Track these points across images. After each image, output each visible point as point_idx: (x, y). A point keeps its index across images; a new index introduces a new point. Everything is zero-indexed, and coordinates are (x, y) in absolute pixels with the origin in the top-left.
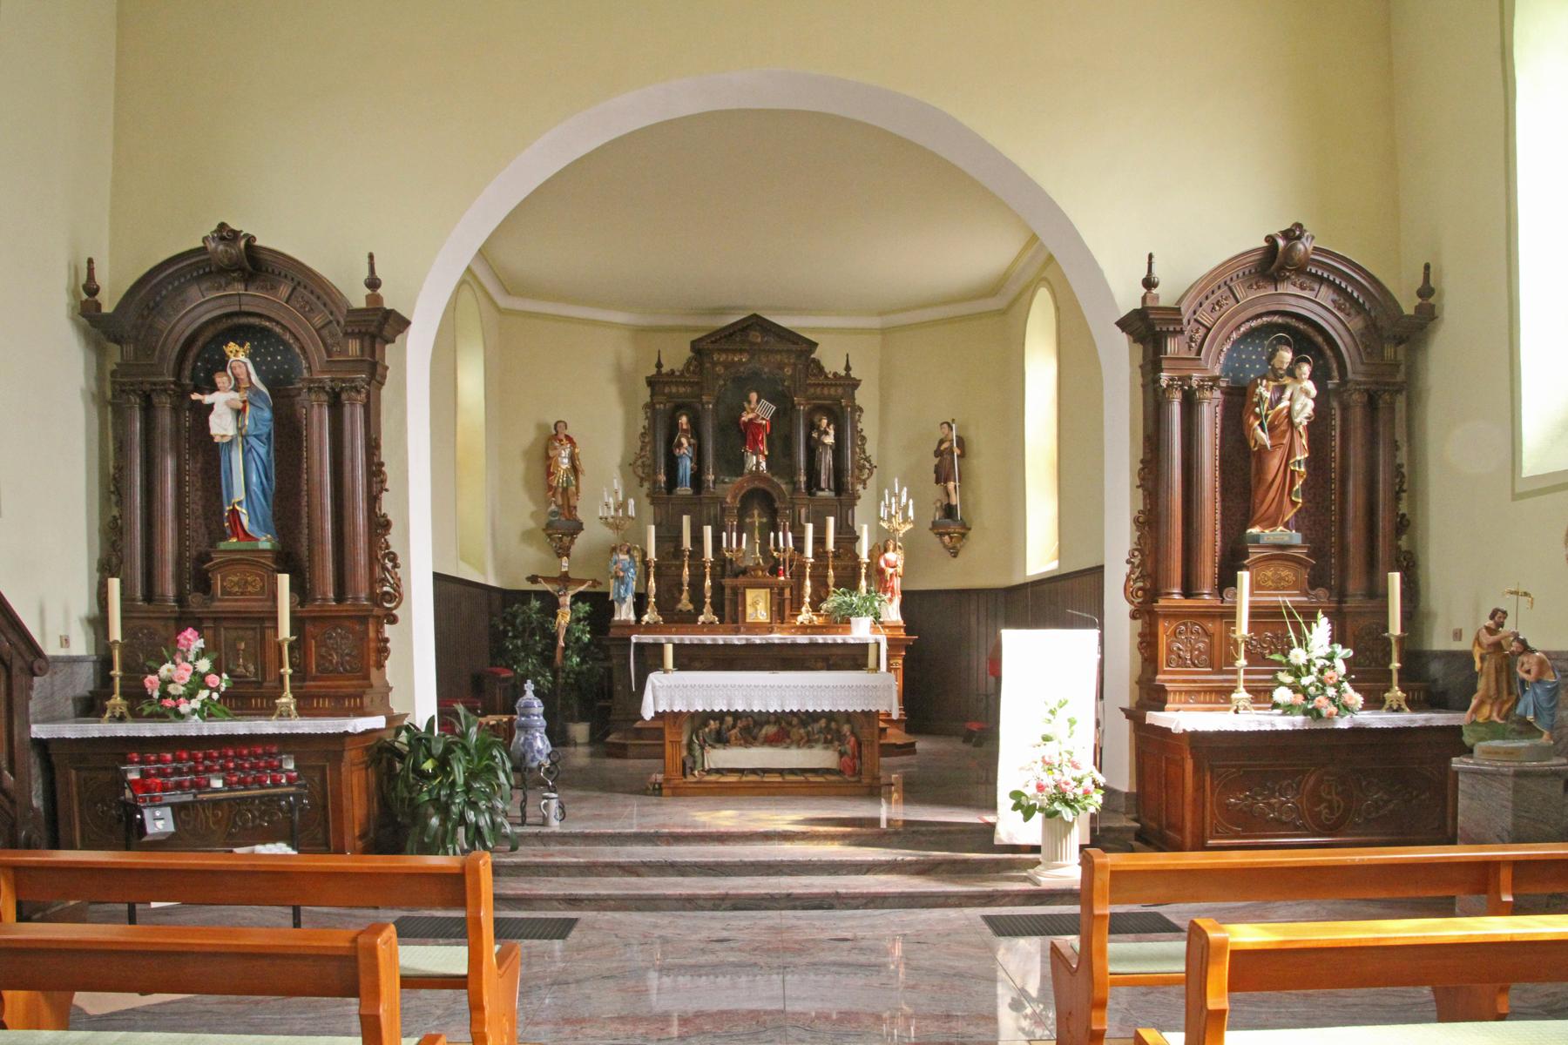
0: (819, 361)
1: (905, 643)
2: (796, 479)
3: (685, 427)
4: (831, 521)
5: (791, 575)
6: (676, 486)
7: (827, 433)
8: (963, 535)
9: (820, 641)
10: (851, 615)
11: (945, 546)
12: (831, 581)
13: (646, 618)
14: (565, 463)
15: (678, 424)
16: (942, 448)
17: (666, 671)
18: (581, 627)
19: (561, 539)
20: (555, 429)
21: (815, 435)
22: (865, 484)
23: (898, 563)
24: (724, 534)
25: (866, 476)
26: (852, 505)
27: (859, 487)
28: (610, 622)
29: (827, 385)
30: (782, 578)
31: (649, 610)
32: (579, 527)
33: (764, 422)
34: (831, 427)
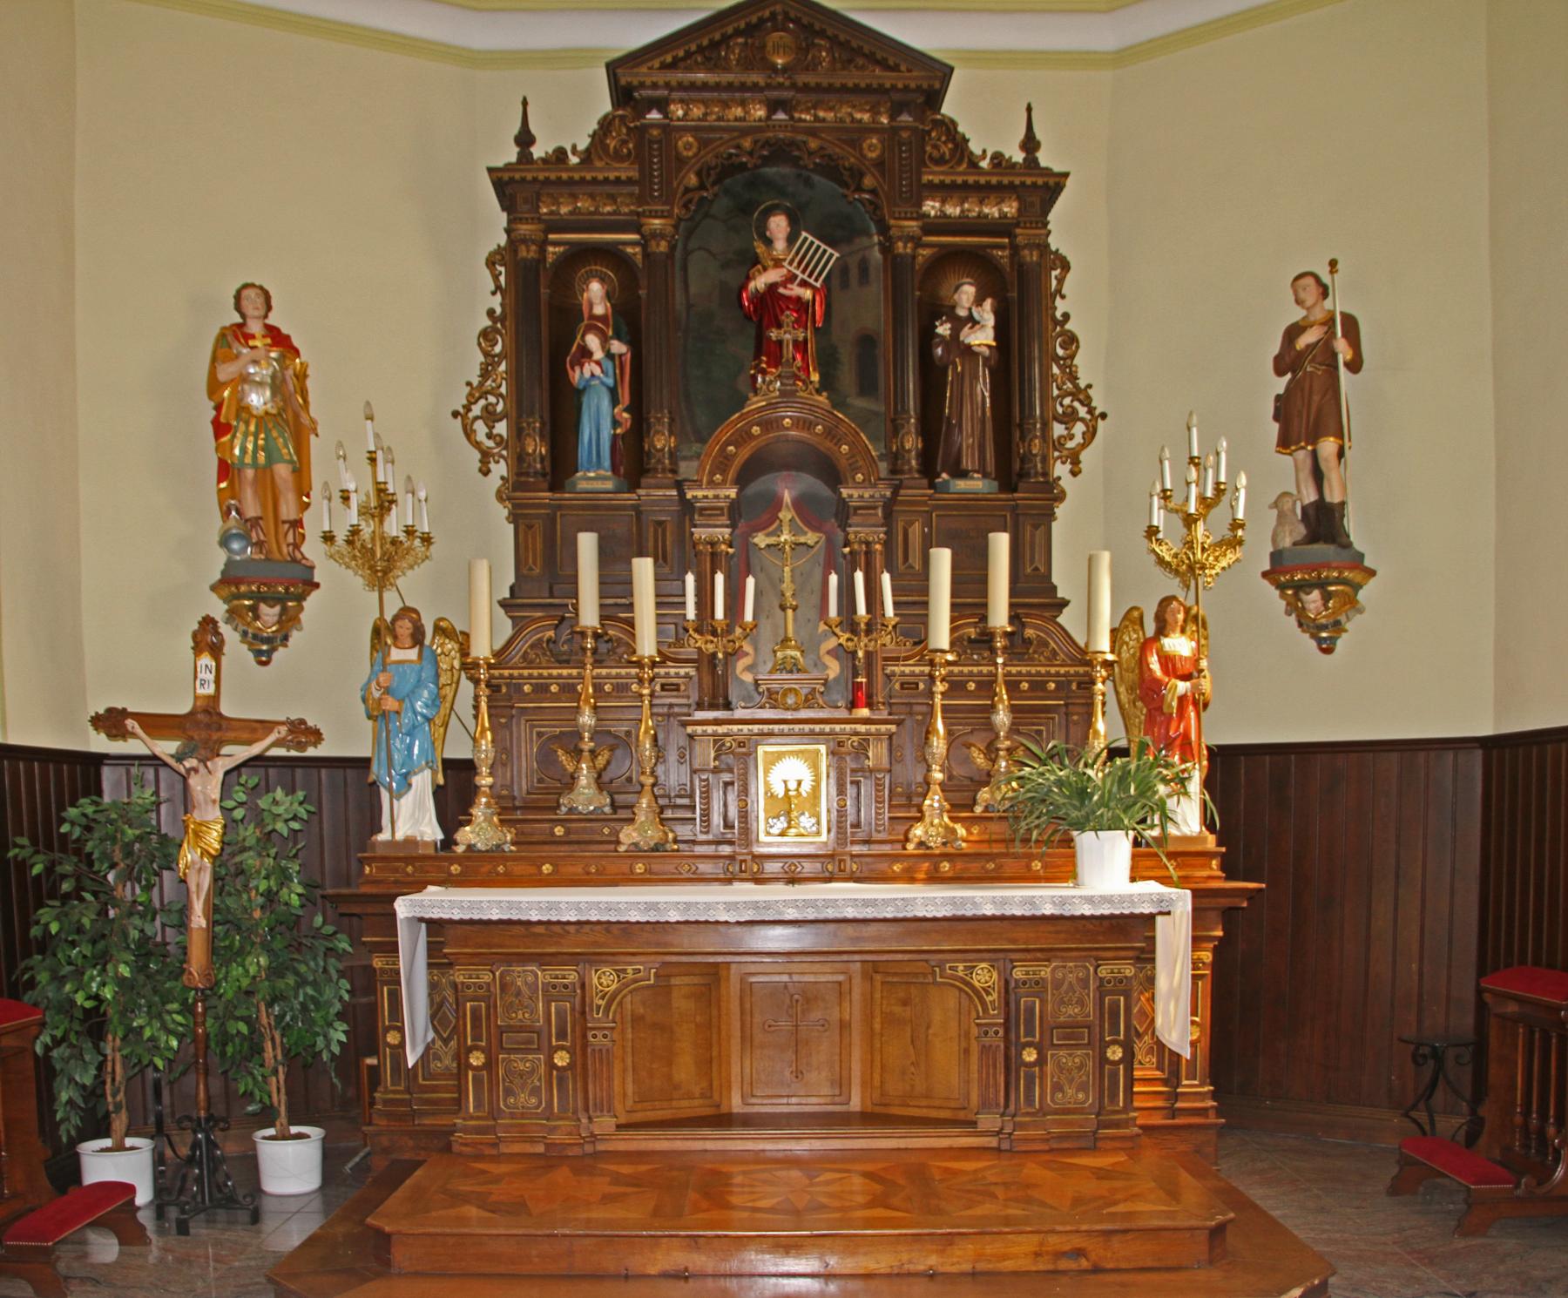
3: (599, 310)
4: (1001, 543)
7: (972, 321)
8: (1357, 587)
12: (1002, 718)
21: (943, 329)
22: (1076, 462)
24: (690, 579)
25: (1078, 439)
27: (1061, 470)
29: (977, 187)
34: (988, 304)
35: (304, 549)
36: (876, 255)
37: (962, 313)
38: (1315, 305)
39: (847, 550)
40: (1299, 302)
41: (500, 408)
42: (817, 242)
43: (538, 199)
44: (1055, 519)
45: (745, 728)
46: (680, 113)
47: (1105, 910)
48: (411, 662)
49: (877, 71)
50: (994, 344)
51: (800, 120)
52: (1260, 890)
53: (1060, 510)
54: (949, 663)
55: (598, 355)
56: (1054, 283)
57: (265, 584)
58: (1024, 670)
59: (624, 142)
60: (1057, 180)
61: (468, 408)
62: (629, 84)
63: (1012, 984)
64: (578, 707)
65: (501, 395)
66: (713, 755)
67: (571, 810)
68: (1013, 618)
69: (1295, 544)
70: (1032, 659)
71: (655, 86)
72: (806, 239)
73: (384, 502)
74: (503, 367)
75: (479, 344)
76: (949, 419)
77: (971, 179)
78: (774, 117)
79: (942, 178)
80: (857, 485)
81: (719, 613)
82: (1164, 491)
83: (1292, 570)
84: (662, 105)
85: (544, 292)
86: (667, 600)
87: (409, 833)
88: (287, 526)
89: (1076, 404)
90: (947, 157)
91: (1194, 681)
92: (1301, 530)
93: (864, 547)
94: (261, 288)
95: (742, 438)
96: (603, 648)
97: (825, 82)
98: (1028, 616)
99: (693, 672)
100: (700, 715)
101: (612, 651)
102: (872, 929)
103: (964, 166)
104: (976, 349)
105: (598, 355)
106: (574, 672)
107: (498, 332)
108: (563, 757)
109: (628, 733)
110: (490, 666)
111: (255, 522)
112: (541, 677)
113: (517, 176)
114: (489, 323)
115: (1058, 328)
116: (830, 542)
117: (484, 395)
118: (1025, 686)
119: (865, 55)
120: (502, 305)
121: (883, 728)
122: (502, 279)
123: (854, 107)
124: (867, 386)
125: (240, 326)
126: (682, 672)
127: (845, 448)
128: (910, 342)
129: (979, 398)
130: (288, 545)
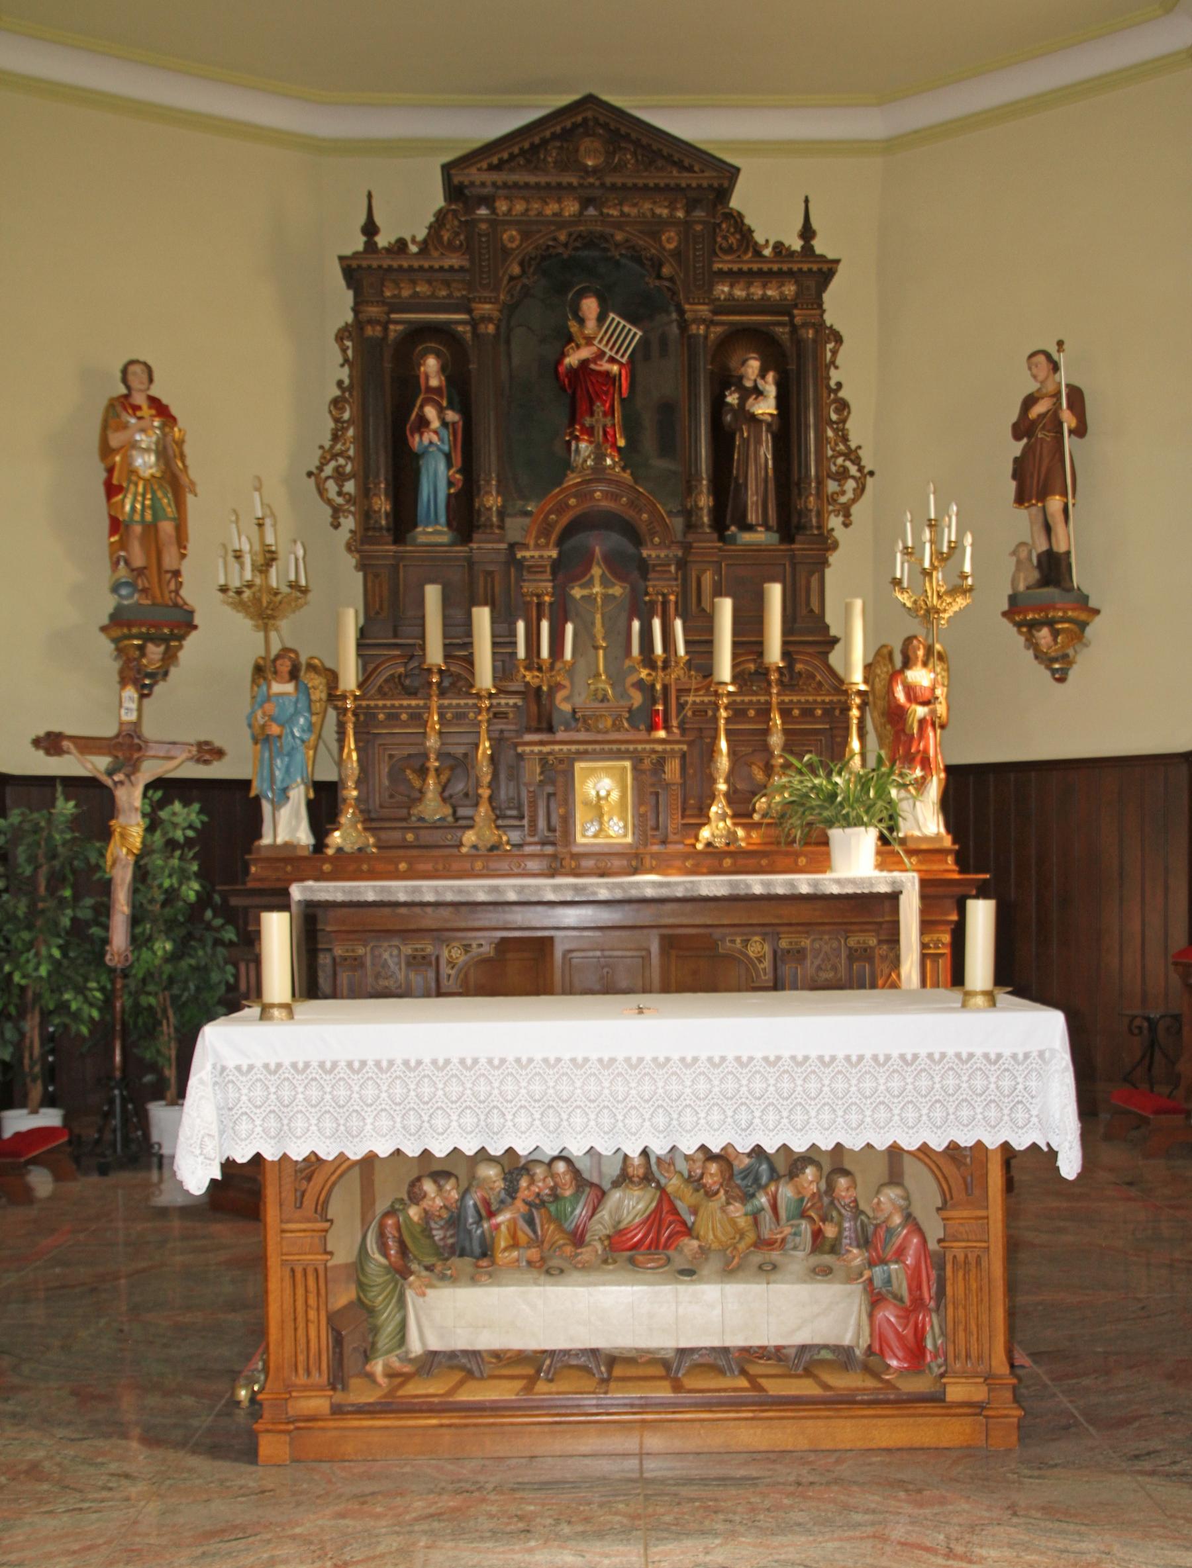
0: (740, 215)
3: (434, 382)
4: (775, 593)
5: (681, 727)
6: (415, 526)
7: (758, 392)
8: (1083, 625)
9: (758, 890)
10: (831, 823)
11: (1039, 656)
12: (776, 740)
14: (146, 463)
15: (417, 377)
17: (265, 1014)
18: (175, 862)
19: (141, 648)
20: (125, 380)
21: (732, 399)
22: (847, 515)
23: (939, 692)
24: (521, 626)
25: (850, 495)
26: (822, 564)
27: (835, 522)
29: (760, 273)
30: (662, 734)
32: (185, 623)
33: (615, 368)
34: (770, 376)
35: (183, 592)
36: (675, 329)
37: (749, 384)
38: (1047, 378)
39: (647, 598)
40: (1035, 377)
41: (348, 469)
42: (623, 323)
43: (383, 285)
44: (829, 565)
45: (565, 748)
46: (504, 208)
47: (850, 890)
48: (287, 694)
49: (675, 173)
50: (775, 412)
51: (608, 215)
52: (985, 881)
53: (833, 558)
54: (730, 694)
55: (435, 424)
56: (829, 355)
57: (154, 626)
58: (795, 699)
59: (457, 234)
60: (830, 266)
61: (321, 469)
62: (461, 183)
63: (779, 953)
64: (425, 733)
65: (349, 458)
66: (538, 770)
67: (421, 819)
68: (786, 655)
69: (1028, 588)
70: (802, 690)
71: (483, 184)
72: (613, 319)
73: (269, 558)
74: (351, 432)
75: (330, 412)
76: (737, 478)
77: (755, 267)
78: (586, 213)
79: (730, 266)
80: (656, 547)
81: (545, 653)
82: (906, 548)
83: (1025, 611)
84: (488, 201)
85: (388, 365)
86: (502, 642)
87: (287, 839)
88: (169, 576)
89: (848, 464)
90: (735, 246)
91: (931, 707)
92: (1035, 575)
93: (660, 598)
94: (145, 364)
95: (562, 508)
96: (446, 684)
97: (630, 182)
98: (798, 653)
99: (520, 703)
100: (528, 737)
101: (453, 684)
102: (669, 907)
103: (750, 254)
104: (762, 417)
105: (435, 424)
106: (421, 703)
107: (346, 401)
108: (410, 775)
109: (466, 755)
110: (356, 698)
111: (140, 572)
112: (393, 706)
113: (364, 264)
114: (338, 393)
115: (832, 396)
116: (634, 590)
117: (334, 457)
118: (796, 712)
119: (663, 157)
120: (351, 377)
121: (676, 747)
122: (350, 353)
123: (654, 203)
124: (667, 447)
125: (126, 397)
126: (511, 702)
127: (645, 516)
128: (703, 420)
129: (763, 460)
130: (171, 592)
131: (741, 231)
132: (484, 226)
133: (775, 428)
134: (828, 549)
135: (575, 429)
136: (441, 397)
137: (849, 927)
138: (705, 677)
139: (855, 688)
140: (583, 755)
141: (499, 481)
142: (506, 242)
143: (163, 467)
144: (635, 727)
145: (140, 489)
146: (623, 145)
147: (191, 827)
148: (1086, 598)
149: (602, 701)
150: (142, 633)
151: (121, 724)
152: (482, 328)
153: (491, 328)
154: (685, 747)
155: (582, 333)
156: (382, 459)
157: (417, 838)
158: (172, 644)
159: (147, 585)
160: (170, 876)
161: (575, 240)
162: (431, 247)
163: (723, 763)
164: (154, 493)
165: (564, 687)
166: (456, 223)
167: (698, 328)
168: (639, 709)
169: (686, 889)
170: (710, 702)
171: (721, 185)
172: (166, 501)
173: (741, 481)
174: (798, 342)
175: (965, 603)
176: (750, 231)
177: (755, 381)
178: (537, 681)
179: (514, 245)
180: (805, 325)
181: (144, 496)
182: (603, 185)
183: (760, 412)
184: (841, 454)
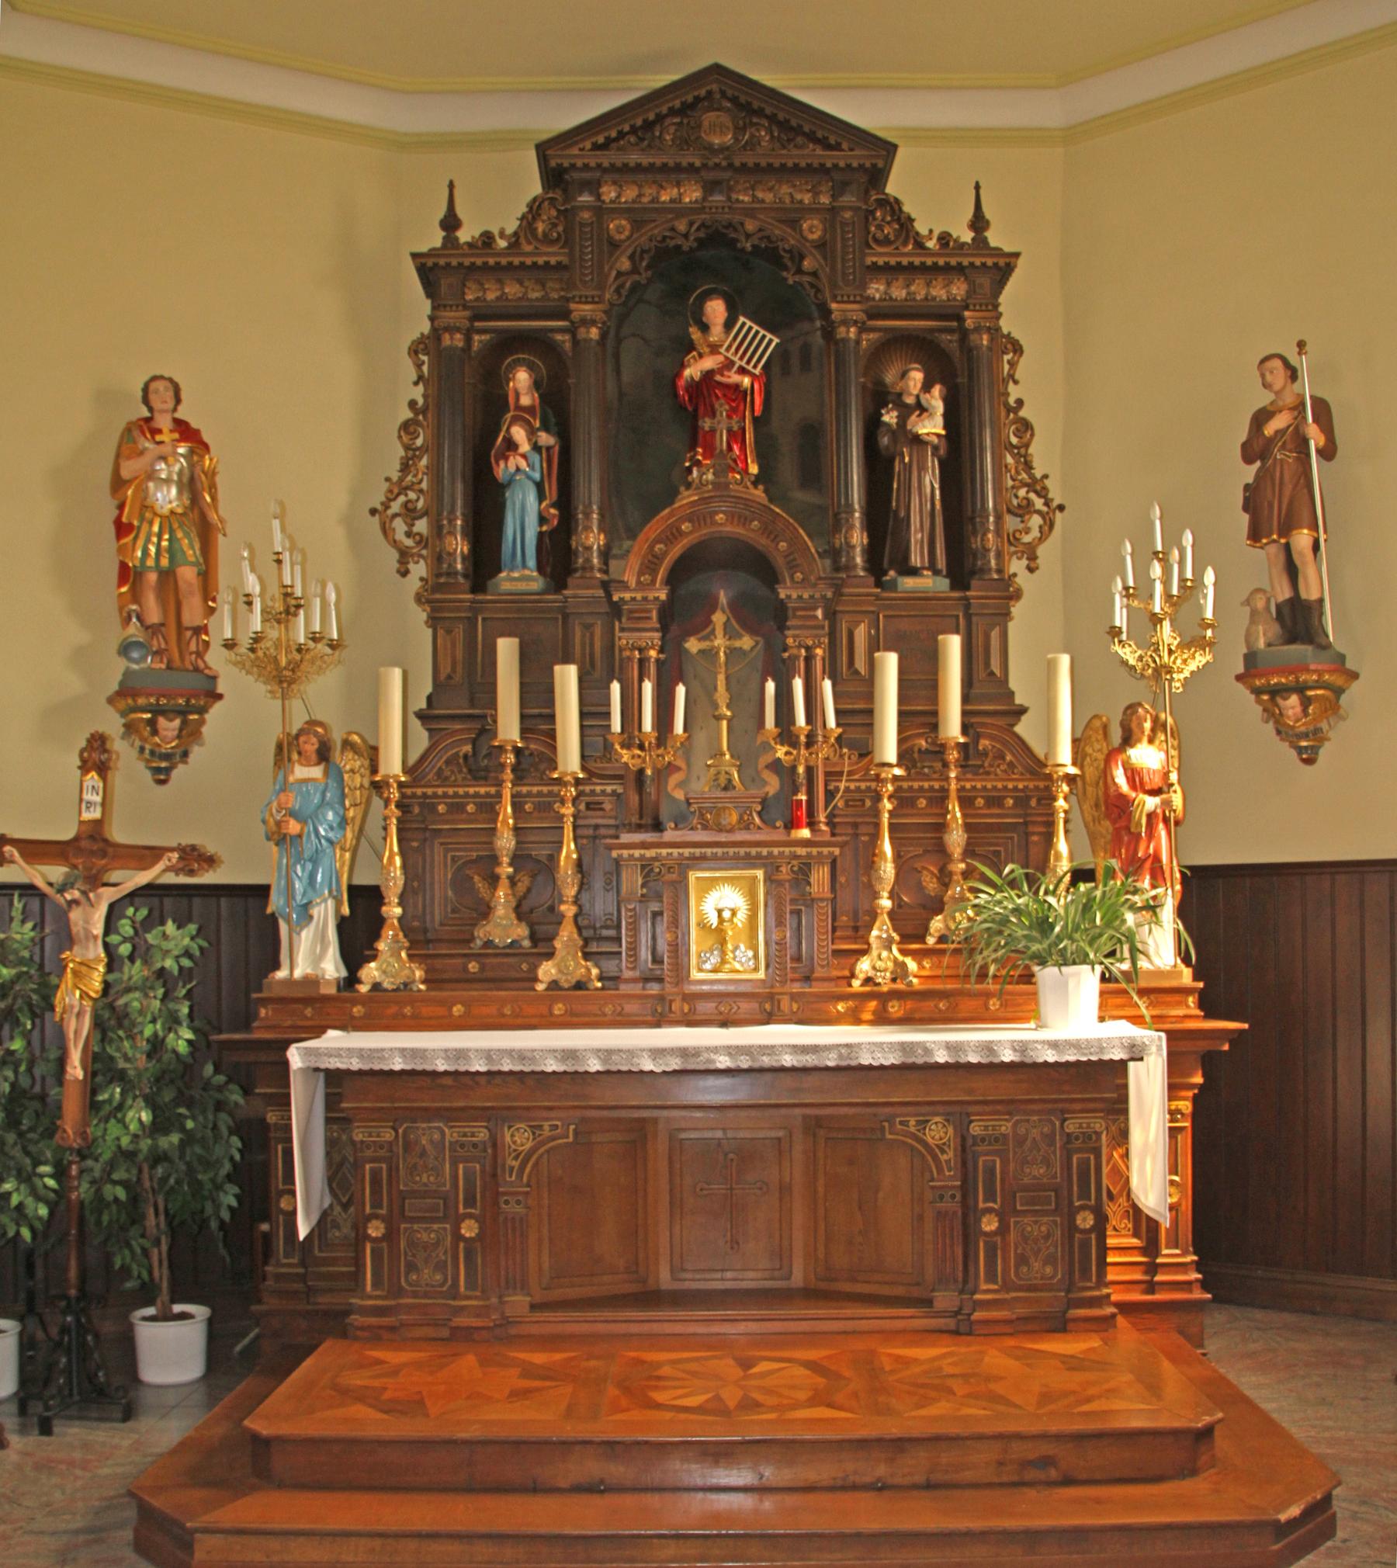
1: (1204, 1046)
2: (839, 541)
3: (525, 401)
4: (953, 645)
6: (500, 571)
7: (921, 408)
8: (1339, 691)
11: (1282, 731)
12: (956, 839)
13: (371, 972)
14: (167, 498)
15: (505, 398)
16: (1269, 430)
19: (152, 723)
20: (146, 400)
21: (890, 417)
22: (1033, 557)
24: (616, 688)
27: (1017, 566)
28: (266, 976)
29: (923, 269)
30: (805, 833)
31: (382, 946)
34: (937, 390)
38: (1284, 388)
39: (786, 655)
41: (420, 504)
42: (756, 328)
44: (1011, 619)
45: (675, 852)
50: (943, 432)
51: (737, 201)
52: (1241, 1032)
53: (1017, 609)
54: (896, 778)
56: (1006, 367)
57: (164, 696)
59: (555, 225)
64: (494, 829)
65: (421, 491)
66: (640, 882)
67: (489, 944)
68: (965, 729)
70: (988, 773)
72: (744, 324)
73: (290, 607)
74: (424, 462)
75: (400, 437)
76: (896, 512)
77: (917, 261)
81: (648, 725)
82: (1126, 588)
84: (593, 187)
86: (593, 712)
87: (309, 971)
88: (189, 634)
89: (1032, 496)
90: (892, 237)
91: (1164, 796)
93: (803, 651)
94: (171, 380)
98: (984, 725)
100: (626, 838)
105: (525, 447)
106: (493, 790)
110: (401, 785)
112: (456, 795)
113: (442, 262)
114: (410, 415)
115: (1012, 416)
116: (769, 646)
117: (404, 490)
119: (804, 134)
120: (425, 396)
121: (825, 850)
122: (425, 368)
126: (609, 789)
129: (928, 490)
131: (898, 220)
132: (586, 215)
133: (942, 452)
134: (1011, 598)
135: (696, 454)
136: (534, 416)
137: (1067, 1106)
138: (862, 756)
139: (1061, 771)
140: (698, 861)
141: (602, 515)
142: (613, 233)
143: (187, 502)
144: (768, 823)
145: (156, 529)
146: (755, 120)
147: (187, 954)
148: (1342, 658)
149: (725, 789)
150: (151, 704)
151: (81, 823)
152: (582, 333)
153: (594, 333)
154: (837, 851)
155: (706, 340)
156: (459, 486)
157: (483, 968)
158: (191, 717)
159: (163, 646)
160: (154, 1021)
161: (698, 229)
162: (522, 240)
163: (888, 870)
164: (172, 532)
165: (679, 769)
166: (554, 213)
167: (848, 332)
168: (777, 796)
169: (840, 1056)
170: (868, 789)
171: (874, 166)
172: (190, 549)
173: (902, 514)
174: (968, 350)
175: (1204, 661)
176: (911, 220)
177: (918, 397)
178: (637, 761)
179: (623, 237)
180: (978, 329)
181: (160, 536)
182: (731, 165)
183: (925, 431)
184: (1024, 484)
